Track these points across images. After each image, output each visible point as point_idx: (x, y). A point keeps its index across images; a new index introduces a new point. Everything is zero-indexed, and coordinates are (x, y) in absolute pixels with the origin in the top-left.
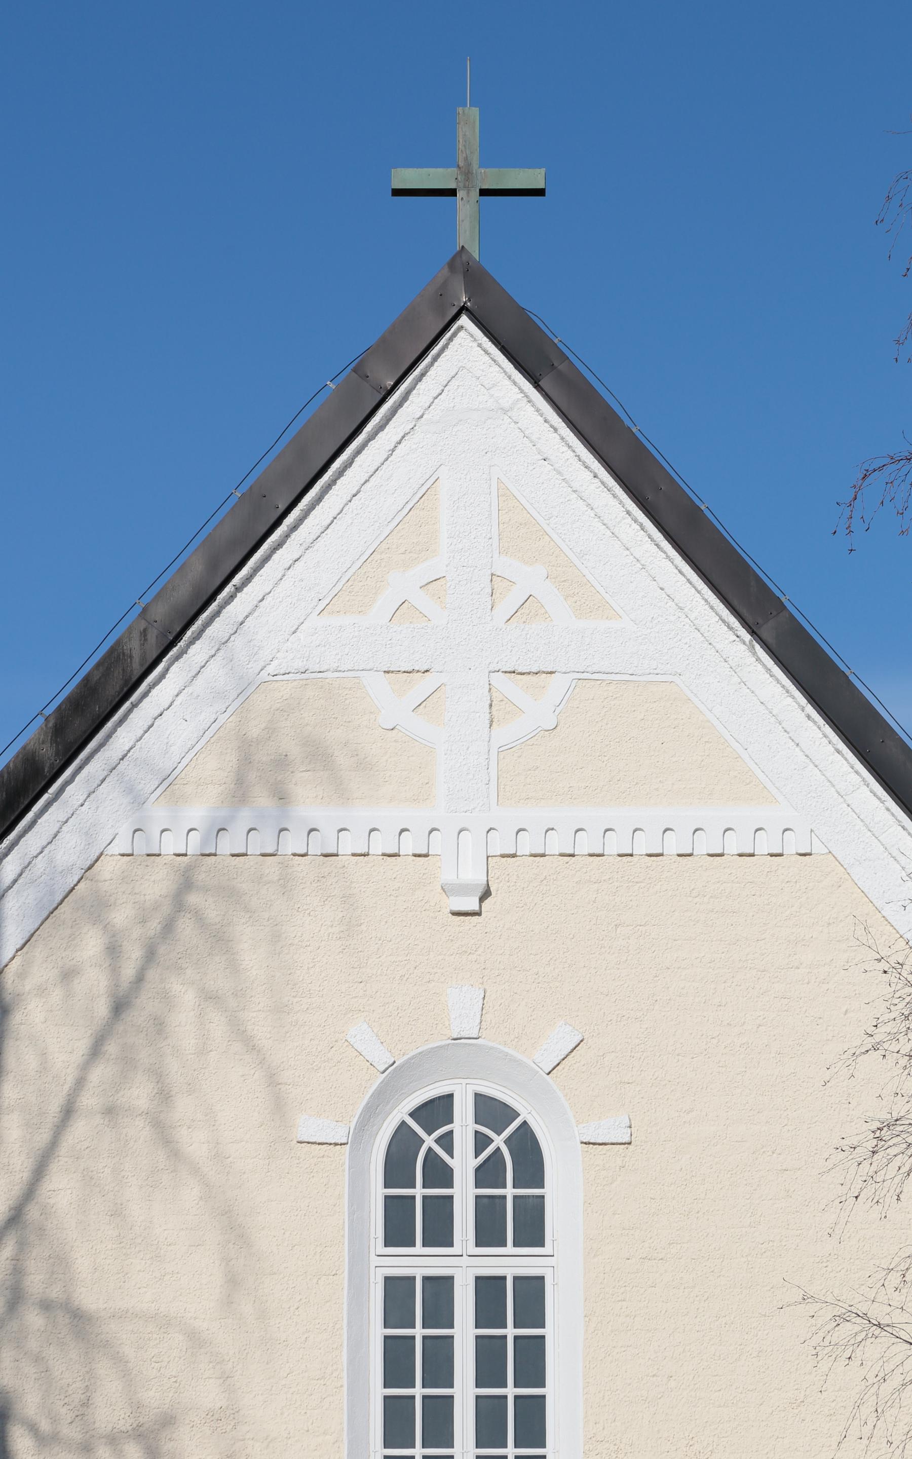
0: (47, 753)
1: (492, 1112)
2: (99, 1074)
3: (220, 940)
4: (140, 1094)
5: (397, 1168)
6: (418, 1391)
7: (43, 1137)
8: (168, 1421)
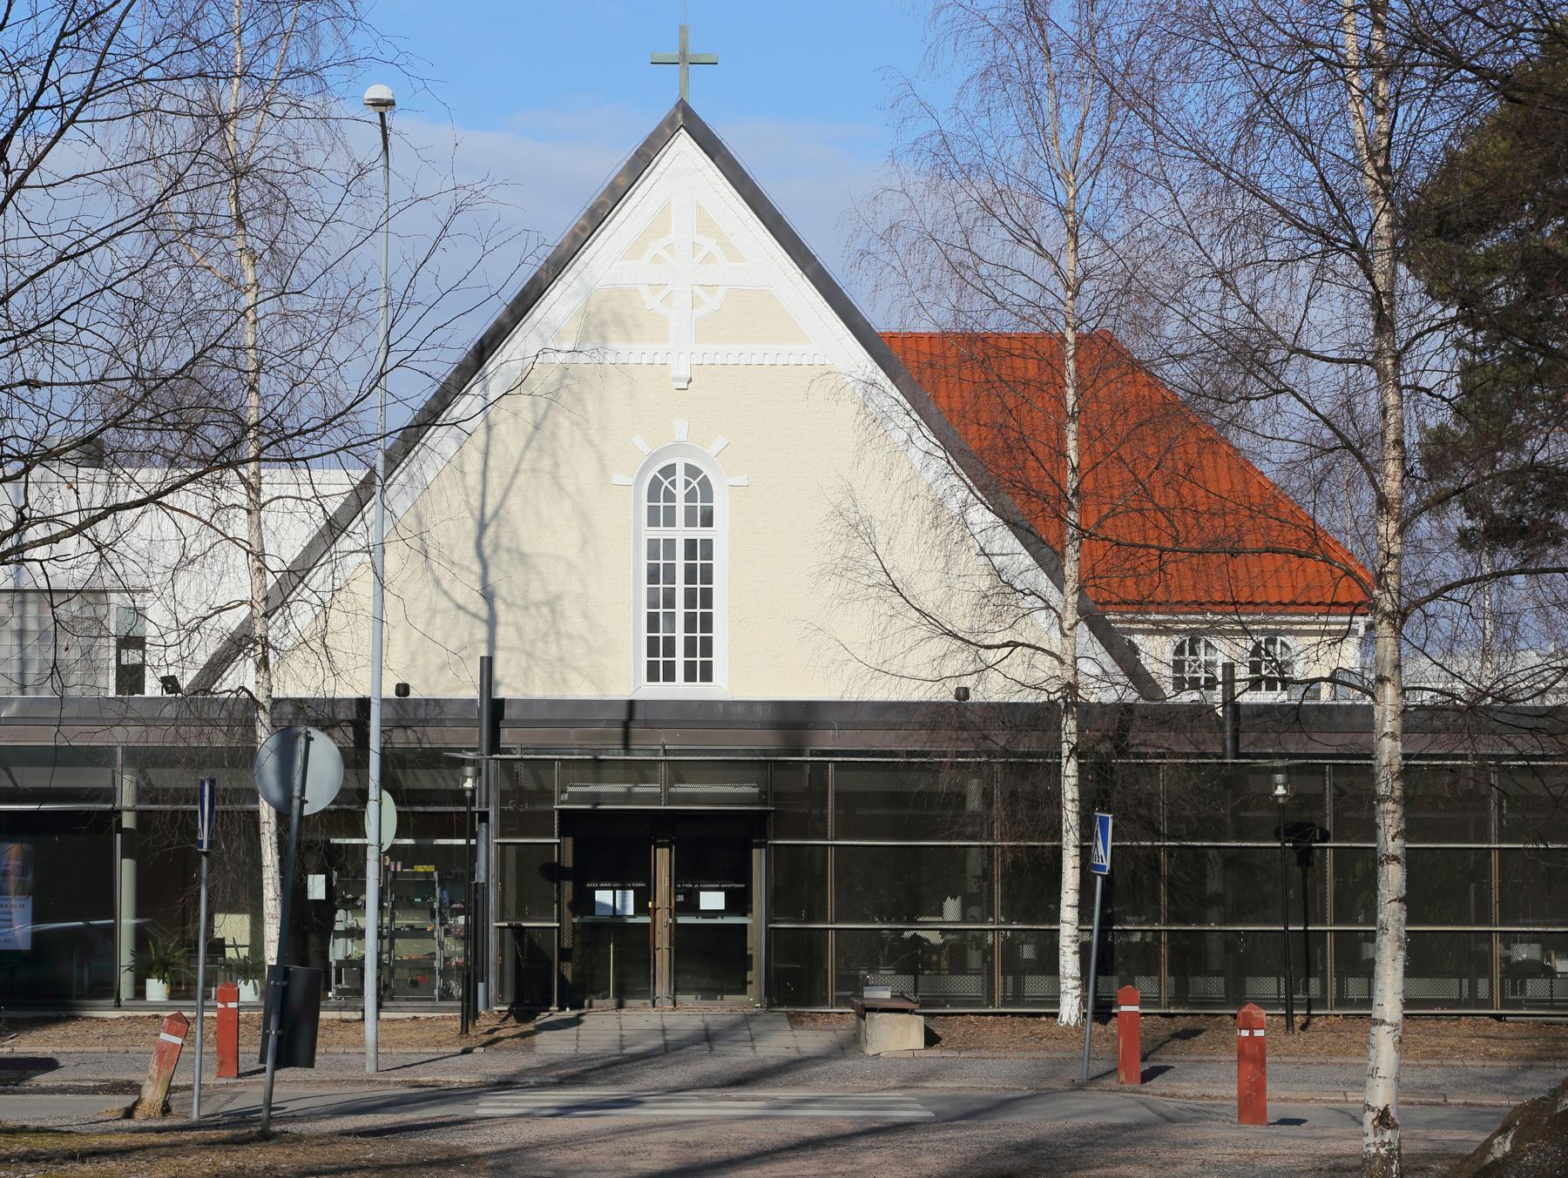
0: (507, 320)
1: (692, 471)
2: (529, 455)
3: (579, 400)
4: (546, 463)
5: (653, 494)
6: (699, 586)
7: (507, 481)
8: (559, 597)
